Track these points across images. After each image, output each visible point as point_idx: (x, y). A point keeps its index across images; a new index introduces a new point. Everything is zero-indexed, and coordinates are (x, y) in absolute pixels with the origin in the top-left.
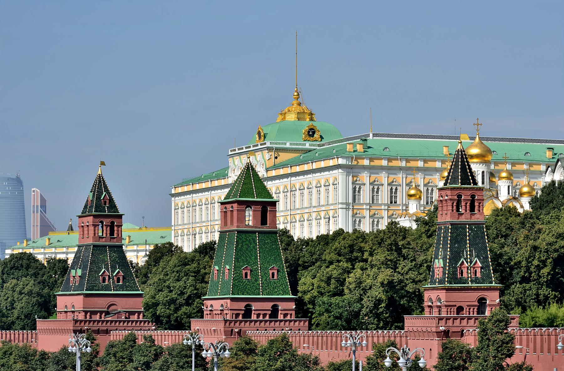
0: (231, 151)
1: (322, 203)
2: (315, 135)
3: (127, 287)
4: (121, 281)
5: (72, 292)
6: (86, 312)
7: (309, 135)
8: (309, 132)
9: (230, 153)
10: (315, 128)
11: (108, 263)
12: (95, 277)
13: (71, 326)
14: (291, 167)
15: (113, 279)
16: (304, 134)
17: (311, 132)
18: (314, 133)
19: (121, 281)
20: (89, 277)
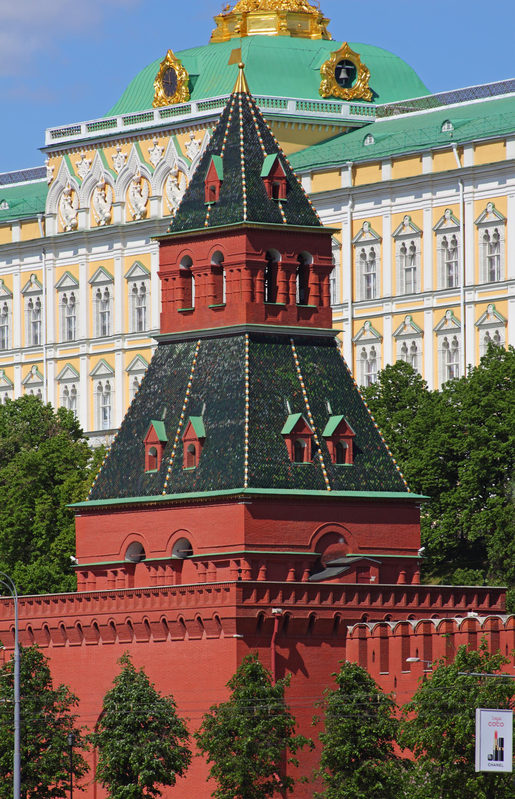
0: (55, 134)
1: (81, 333)
2: (357, 83)
3: (367, 478)
4: (348, 455)
5: (165, 497)
6: (254, 561)
7: (339, 81)
8: (338, 71)
9: (49, 141)
10: (353, 59)
11: (300, 396)
12: (272, 442)
13: (227, 606)
14: (355, 167)
15: (325, 450)
16: (324, 76)
17: (345, 71)
18: (352, 74)
19: (348, 455)
20: (252, 441)
